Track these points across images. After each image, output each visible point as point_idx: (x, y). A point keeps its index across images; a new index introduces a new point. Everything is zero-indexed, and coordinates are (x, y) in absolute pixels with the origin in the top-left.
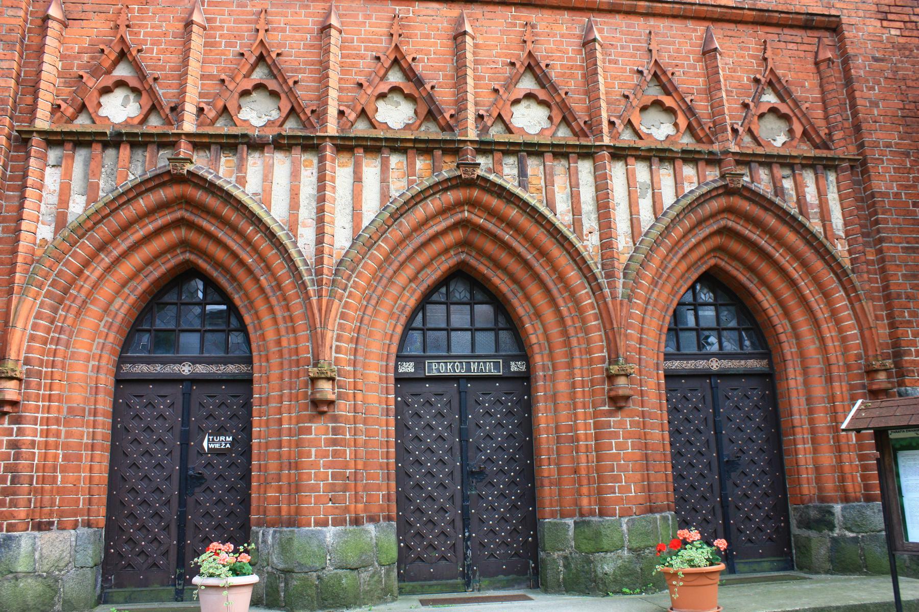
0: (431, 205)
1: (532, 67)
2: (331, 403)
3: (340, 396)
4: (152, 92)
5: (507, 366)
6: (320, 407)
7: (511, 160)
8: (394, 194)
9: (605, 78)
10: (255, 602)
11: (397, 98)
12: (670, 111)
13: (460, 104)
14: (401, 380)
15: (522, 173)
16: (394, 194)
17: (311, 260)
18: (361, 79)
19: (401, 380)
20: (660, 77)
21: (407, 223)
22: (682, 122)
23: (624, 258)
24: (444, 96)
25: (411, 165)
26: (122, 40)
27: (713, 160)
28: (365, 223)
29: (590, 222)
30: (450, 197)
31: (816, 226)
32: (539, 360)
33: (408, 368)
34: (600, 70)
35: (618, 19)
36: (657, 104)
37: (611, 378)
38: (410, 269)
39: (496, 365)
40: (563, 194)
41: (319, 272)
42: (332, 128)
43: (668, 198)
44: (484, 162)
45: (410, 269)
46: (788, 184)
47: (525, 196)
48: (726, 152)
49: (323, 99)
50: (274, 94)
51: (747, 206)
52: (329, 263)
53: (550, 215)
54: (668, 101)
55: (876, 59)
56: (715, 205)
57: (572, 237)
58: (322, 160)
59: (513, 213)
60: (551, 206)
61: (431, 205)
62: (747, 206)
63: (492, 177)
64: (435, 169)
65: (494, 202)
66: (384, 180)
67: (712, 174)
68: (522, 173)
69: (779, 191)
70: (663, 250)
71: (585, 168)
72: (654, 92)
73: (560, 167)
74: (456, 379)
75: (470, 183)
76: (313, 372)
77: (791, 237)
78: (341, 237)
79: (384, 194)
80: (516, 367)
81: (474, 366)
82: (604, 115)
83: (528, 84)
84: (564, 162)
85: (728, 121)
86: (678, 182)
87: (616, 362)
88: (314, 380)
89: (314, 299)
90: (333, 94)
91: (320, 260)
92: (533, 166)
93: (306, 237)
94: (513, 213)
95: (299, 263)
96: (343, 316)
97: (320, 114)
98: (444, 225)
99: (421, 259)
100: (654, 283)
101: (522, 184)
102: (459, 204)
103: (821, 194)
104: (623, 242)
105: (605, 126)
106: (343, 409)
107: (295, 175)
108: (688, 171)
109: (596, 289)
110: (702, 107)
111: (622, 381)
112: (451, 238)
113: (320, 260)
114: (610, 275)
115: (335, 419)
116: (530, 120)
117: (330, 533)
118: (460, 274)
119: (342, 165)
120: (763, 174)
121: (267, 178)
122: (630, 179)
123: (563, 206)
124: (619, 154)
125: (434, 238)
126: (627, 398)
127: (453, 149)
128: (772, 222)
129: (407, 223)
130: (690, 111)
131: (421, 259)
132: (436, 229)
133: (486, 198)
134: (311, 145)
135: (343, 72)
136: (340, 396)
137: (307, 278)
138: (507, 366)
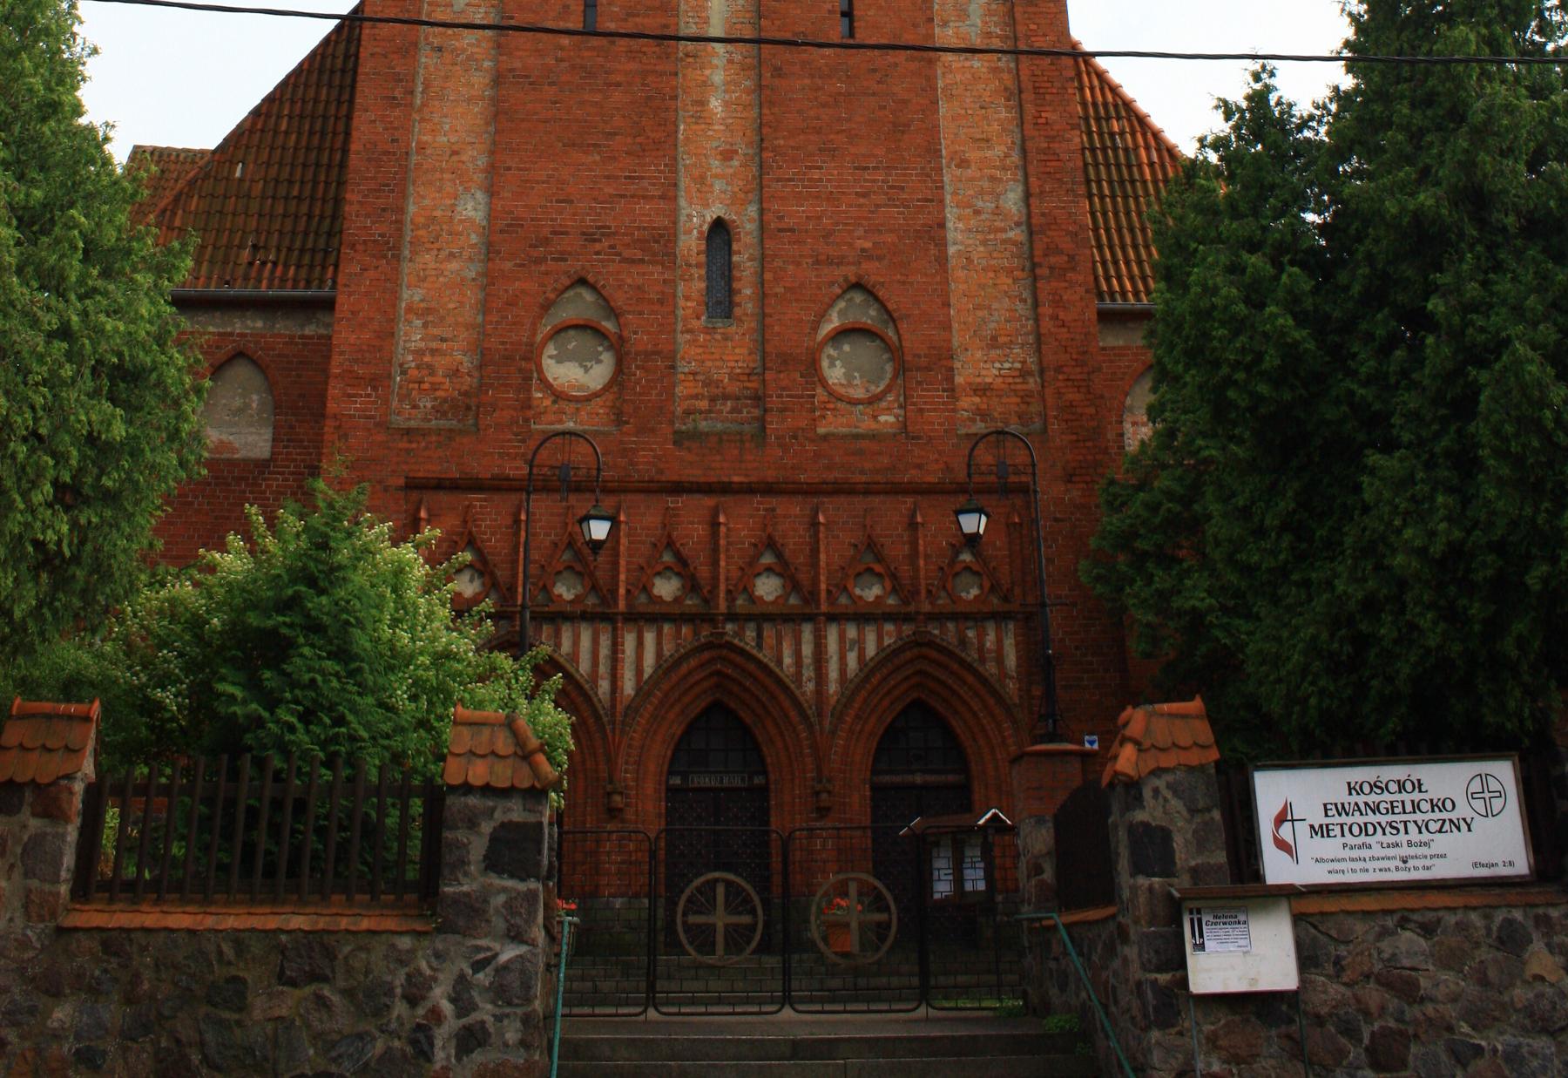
0: (693, 662)
1: (771, 544)
2: (620, 810)
3: (627, 805)
4: (492, 574)
5: (751, 779)
6: (613, 813)
7: (752, 625)
8: (667, 653)
9: (827, 553)
10: (619, 954)
11: (668, 573)
12: (879, 575)
13: (715, 579)
14: (671, 790)
15: (760, 636)
16: (667, 653)
17: (607, 704)
18: (642, 561)
19: (671, 790)
20: (871, 545)
21: (674, 678)
22: (888, 584)
23: (833, 701)
24: (704, 572)
25: (679, 632)
26: (470, 533)
27: (908, 618)
28: (646, 676)
29: (808, 672)
30: (706, 655)
31: (991, 668)
32: (772, 777)
33: (677, 781)
34: (822, 548)
35: (842, 499)
36: (869, 570)
37: (817, 793)
38: (677, 708)
39: (743, 780)
40: (789, 653)
41: (613, 715)
42: (622, 605)
43: (871, 650)
44: (729, 627)
45: (677, 708)
46: (971, 634)
47: (760, 656)
48: (918, 613)
49: (615, 577)
50: (579, 574)
51: (934, 654)
52: (620, 708)
53: (777, 670)
54: (878, 568)
55: (1056, 520)
56: (908, 655)
57: (793, 686)
58: (615, 629)
59: (751, 667)
60: (780, 662)
61: (693, 662)
62: (934, 654)
63: (736, 641)
64: (696, 633)
65: (738, 659)
66: (659, 644)
67: (907, 629)
68: (760, 636)
69: (963, 642)
70: (864, 693)
71: (807, 632)
72: (868, 559)
73: (787, 630)
74: (709, 789)
75: (720, 646)
76: (609, 788)
77: (970, 679)
78: (629, 687)
79: (659, 653)
80: (758, 780)
81: (726, 780)
82: (823, 586)
83: (768, 559)
84: (791, 625)
85: (923, 582)
86: (880, 638)
87: (820, 781)
88: (609, 794)
89: (608, 728)
90: (622, 577)
91: (613, 706)
92: (769, 631)
93: (604, 686)
94: (751, 667)
95: (599, 706)
96: (630, 746)
97: (614, 591)
98: (703, 675)
99: (686, 700)
100: (857, 717)
101: (760, 646)
102: (712, 660)
103: (999, 641)
104: (833, 688)
105: (823, 595)
106: (630, 815)
107: (595, 642)
108: (889, 627)
109: (810, 726)
110: (905, 570)
111: (824, 796)
112: (706, 684)
113: (613, 706)
114: (820, 715)
115: (623, 821)
116: (767, 588)
117: (618, 903)
118: (716, 708)
119: (629, 631)
120: (951, 626)
121: (576, 643)
122: (842, 637)
123: (788, 660)
124: (832, 618)
125: (697, 683)
126: (828, 809)
127: (710, 619)
128: (955, 666)
129: (674, 678)
130: (894, 577)
131: (686, 700)
132: (697, 677)
133: (732, 656)
134: (609, 618)
135: (630, 556)
136: (627, 805)
137: (605, 719)
138: (751, 779)
